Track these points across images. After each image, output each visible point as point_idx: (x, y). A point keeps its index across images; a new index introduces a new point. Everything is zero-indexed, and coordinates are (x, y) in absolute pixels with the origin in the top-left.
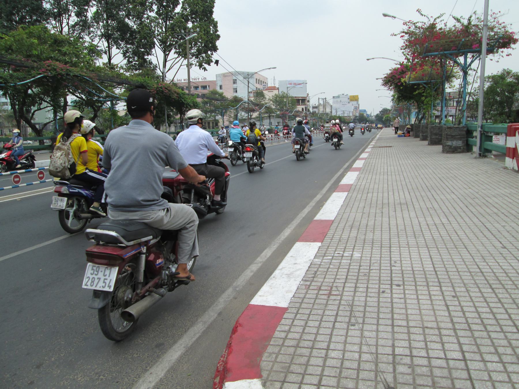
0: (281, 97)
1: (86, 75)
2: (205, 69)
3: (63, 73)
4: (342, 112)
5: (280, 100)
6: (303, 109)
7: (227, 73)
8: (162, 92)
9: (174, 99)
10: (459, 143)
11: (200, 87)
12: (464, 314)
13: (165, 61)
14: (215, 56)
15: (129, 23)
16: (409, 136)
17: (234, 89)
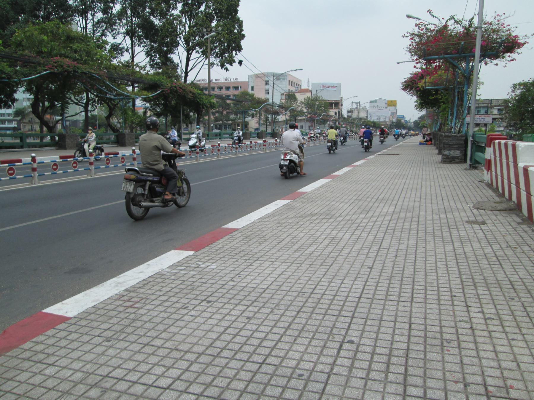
0: (313, 100)
1: (95, 72)
2: (227, 69)
3: (70, 69)
4: (377, 117)
5: (311, 103)
6: (336, 113)
7: (259, 74)
8: (176, 91)
9: (190, 99)
10: (456, 153)
11: (216, 88)
12: (520, 330)
13: (188, 60)
14: (238, 57)
15: (154, 21)
16: (431, 144)
17: (266, 90)
